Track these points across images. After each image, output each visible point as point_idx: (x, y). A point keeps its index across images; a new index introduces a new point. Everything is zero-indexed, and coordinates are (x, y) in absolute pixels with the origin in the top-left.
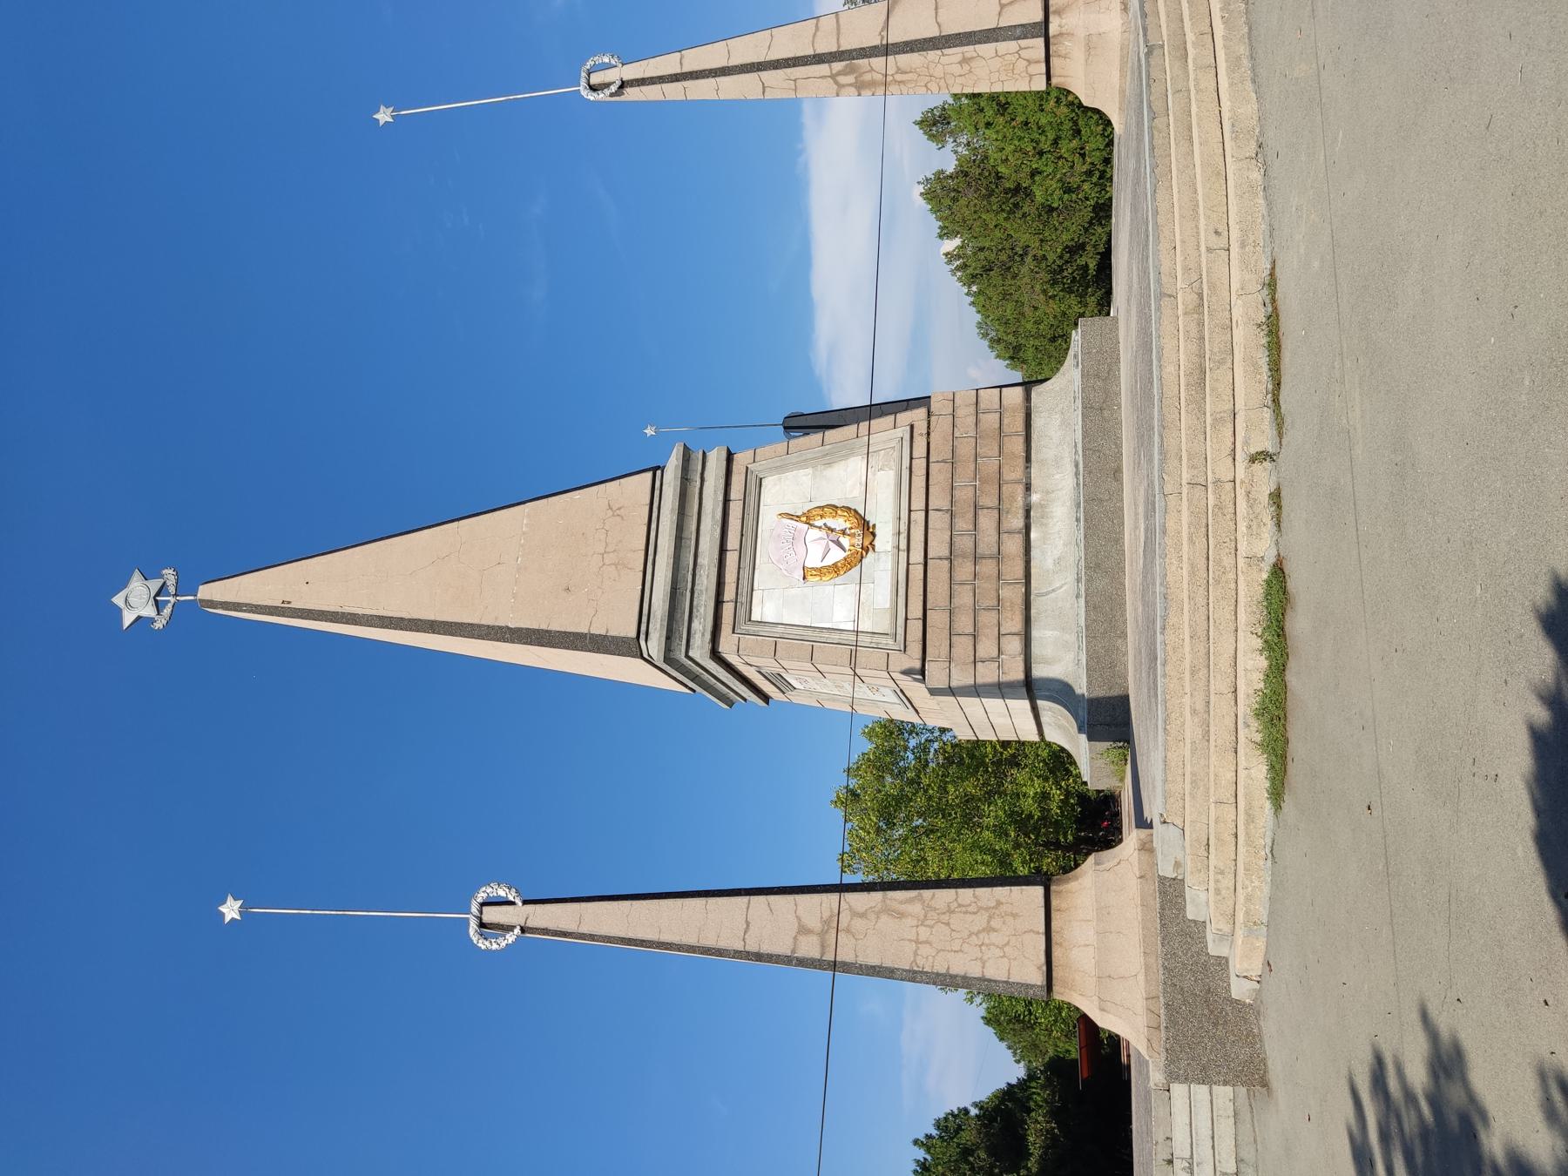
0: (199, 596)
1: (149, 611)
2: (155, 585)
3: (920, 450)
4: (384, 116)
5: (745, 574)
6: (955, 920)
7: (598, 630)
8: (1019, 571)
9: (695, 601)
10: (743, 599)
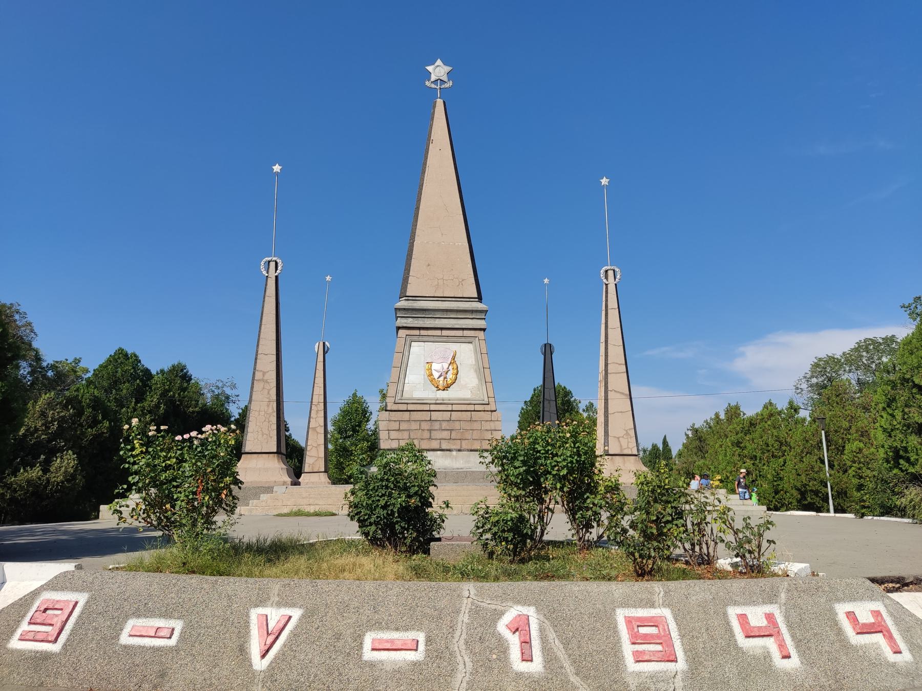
0: (438, 100)
1: (433, 78)
2: (445, 78)
3: (478, 408)
4: (604, 181)
5: (432, 339)
6: (266, 423)
7: (411, 279)
9: (423, 320)
10: (421, 339)
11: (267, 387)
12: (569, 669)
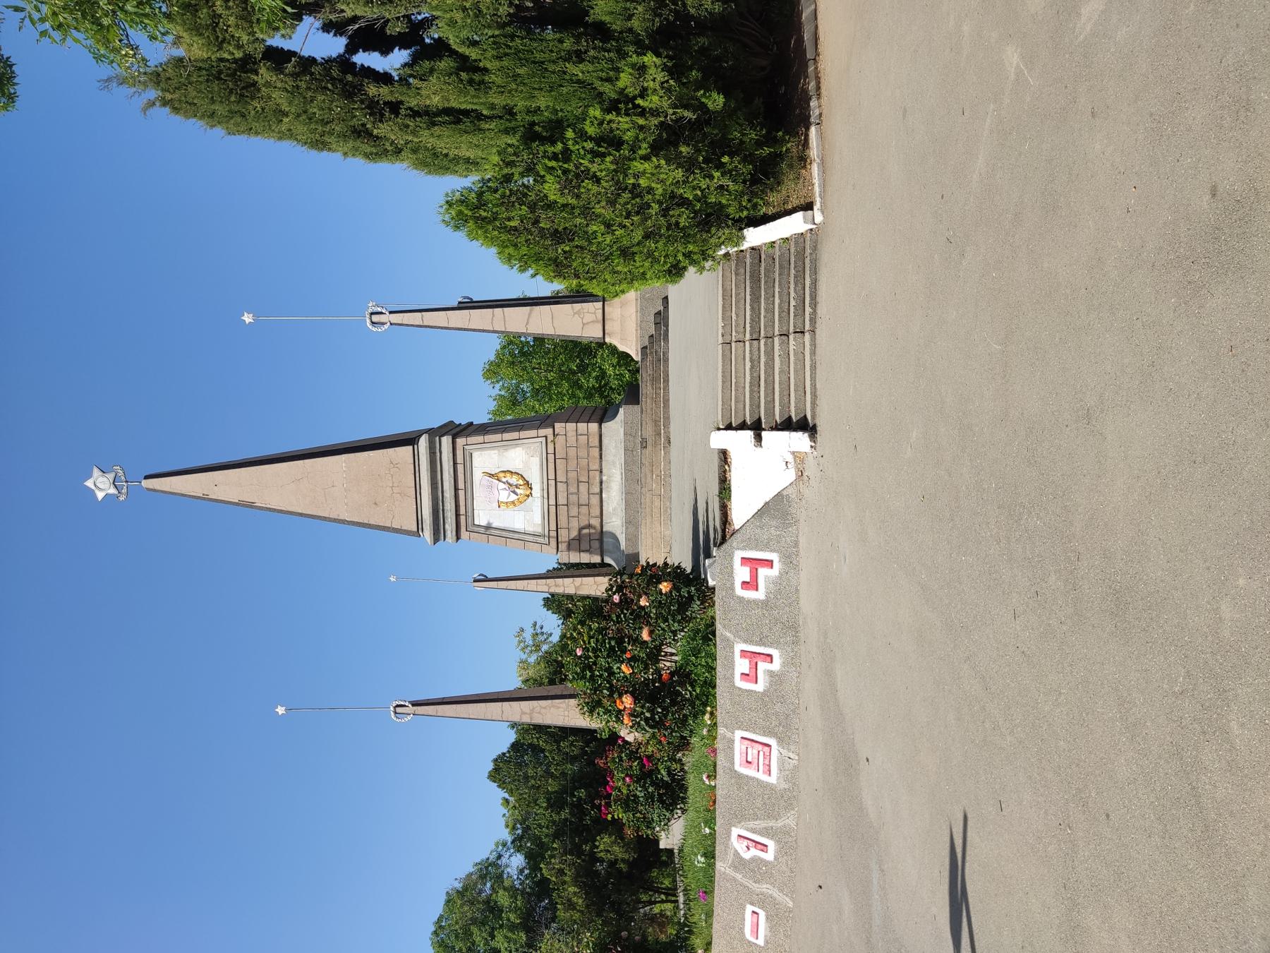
3: (551, 450)
8: (598, 513)
10: (470, 514)
11: (538, 709)
12: (771, 823)
